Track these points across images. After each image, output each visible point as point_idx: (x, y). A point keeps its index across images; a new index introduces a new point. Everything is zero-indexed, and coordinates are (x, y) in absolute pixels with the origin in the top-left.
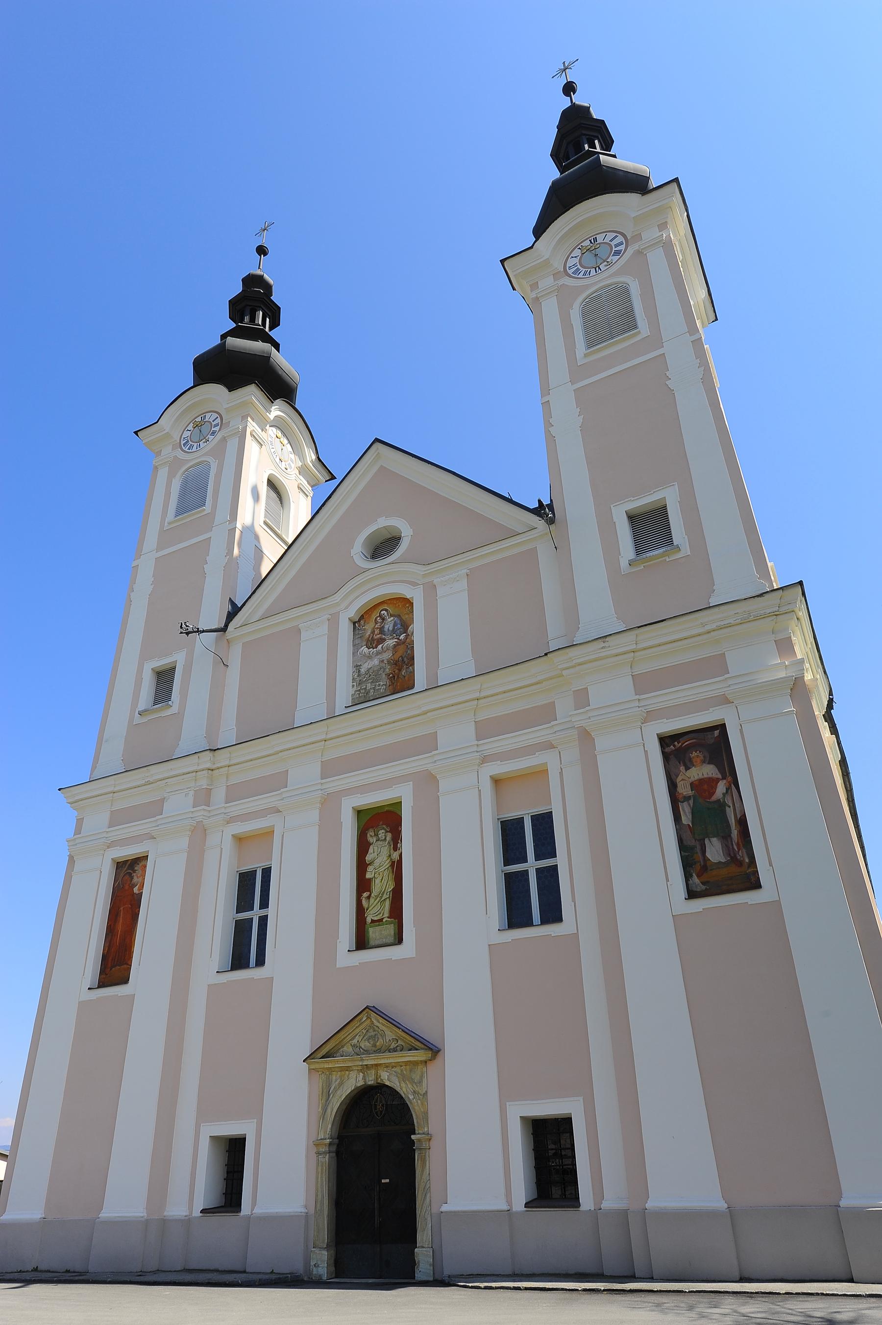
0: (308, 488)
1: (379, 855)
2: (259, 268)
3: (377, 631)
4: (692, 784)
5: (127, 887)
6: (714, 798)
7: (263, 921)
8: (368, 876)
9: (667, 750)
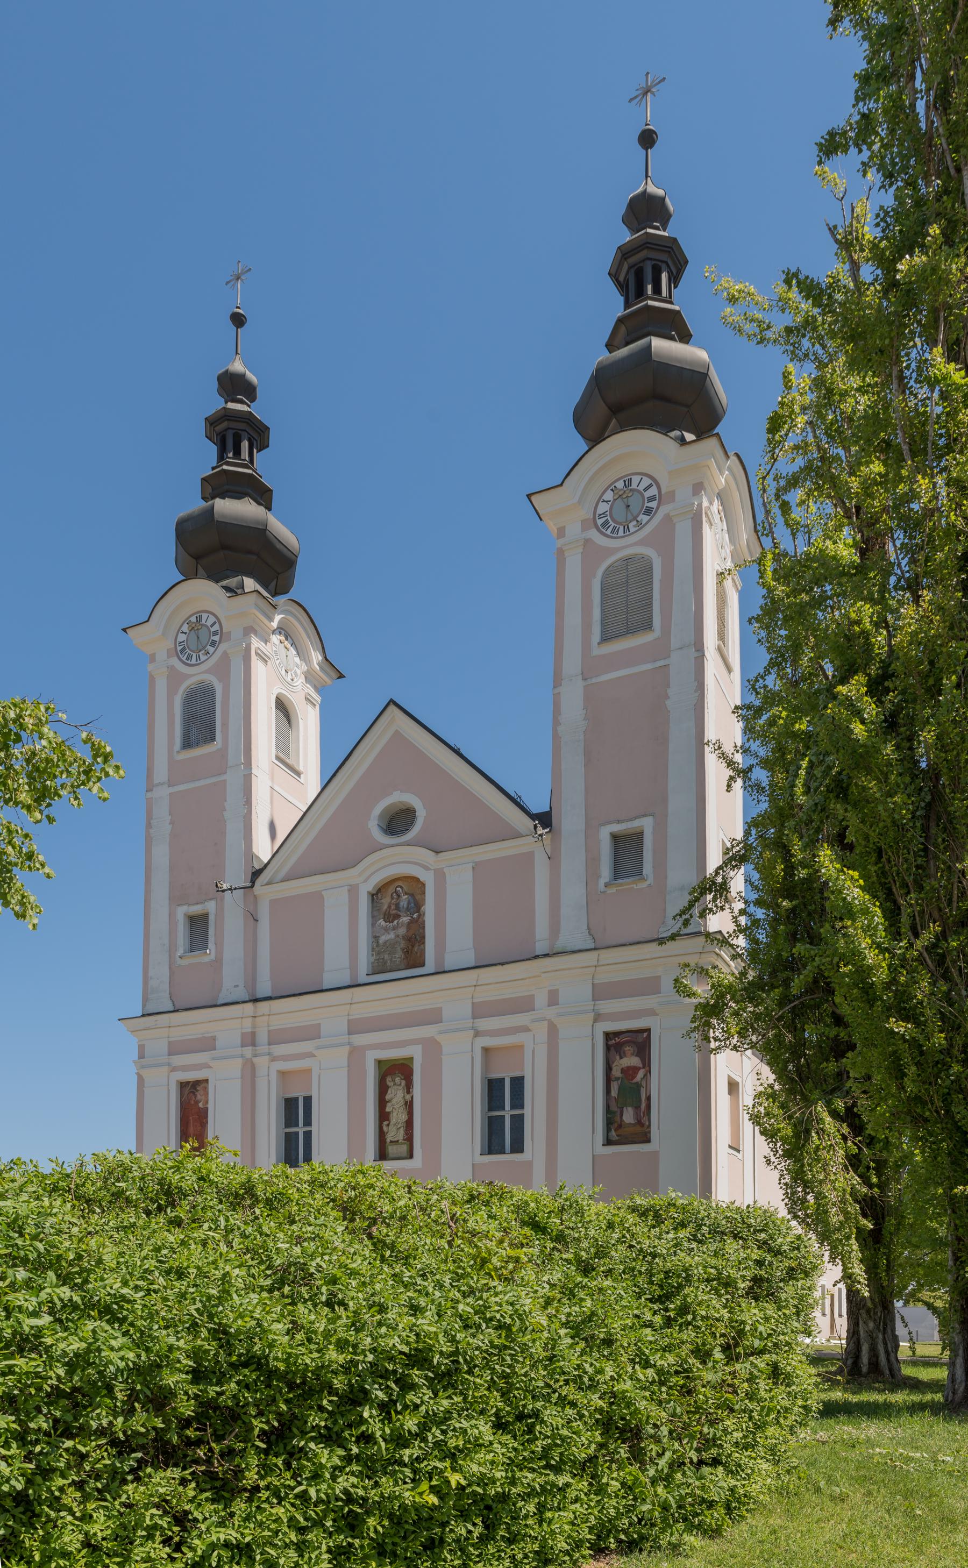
0: (317, 698)
1: (396, 1095)
2: (237, 353)
3: (393, 907)
4: (622, 1069)
5: (192, 1102)
6: (635, 1080)
7: (308, 1135)
8: (388, 1110)
9: (611, 1043)
